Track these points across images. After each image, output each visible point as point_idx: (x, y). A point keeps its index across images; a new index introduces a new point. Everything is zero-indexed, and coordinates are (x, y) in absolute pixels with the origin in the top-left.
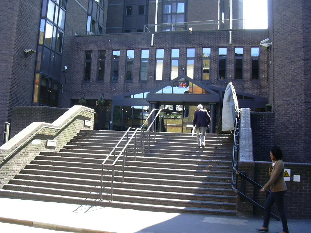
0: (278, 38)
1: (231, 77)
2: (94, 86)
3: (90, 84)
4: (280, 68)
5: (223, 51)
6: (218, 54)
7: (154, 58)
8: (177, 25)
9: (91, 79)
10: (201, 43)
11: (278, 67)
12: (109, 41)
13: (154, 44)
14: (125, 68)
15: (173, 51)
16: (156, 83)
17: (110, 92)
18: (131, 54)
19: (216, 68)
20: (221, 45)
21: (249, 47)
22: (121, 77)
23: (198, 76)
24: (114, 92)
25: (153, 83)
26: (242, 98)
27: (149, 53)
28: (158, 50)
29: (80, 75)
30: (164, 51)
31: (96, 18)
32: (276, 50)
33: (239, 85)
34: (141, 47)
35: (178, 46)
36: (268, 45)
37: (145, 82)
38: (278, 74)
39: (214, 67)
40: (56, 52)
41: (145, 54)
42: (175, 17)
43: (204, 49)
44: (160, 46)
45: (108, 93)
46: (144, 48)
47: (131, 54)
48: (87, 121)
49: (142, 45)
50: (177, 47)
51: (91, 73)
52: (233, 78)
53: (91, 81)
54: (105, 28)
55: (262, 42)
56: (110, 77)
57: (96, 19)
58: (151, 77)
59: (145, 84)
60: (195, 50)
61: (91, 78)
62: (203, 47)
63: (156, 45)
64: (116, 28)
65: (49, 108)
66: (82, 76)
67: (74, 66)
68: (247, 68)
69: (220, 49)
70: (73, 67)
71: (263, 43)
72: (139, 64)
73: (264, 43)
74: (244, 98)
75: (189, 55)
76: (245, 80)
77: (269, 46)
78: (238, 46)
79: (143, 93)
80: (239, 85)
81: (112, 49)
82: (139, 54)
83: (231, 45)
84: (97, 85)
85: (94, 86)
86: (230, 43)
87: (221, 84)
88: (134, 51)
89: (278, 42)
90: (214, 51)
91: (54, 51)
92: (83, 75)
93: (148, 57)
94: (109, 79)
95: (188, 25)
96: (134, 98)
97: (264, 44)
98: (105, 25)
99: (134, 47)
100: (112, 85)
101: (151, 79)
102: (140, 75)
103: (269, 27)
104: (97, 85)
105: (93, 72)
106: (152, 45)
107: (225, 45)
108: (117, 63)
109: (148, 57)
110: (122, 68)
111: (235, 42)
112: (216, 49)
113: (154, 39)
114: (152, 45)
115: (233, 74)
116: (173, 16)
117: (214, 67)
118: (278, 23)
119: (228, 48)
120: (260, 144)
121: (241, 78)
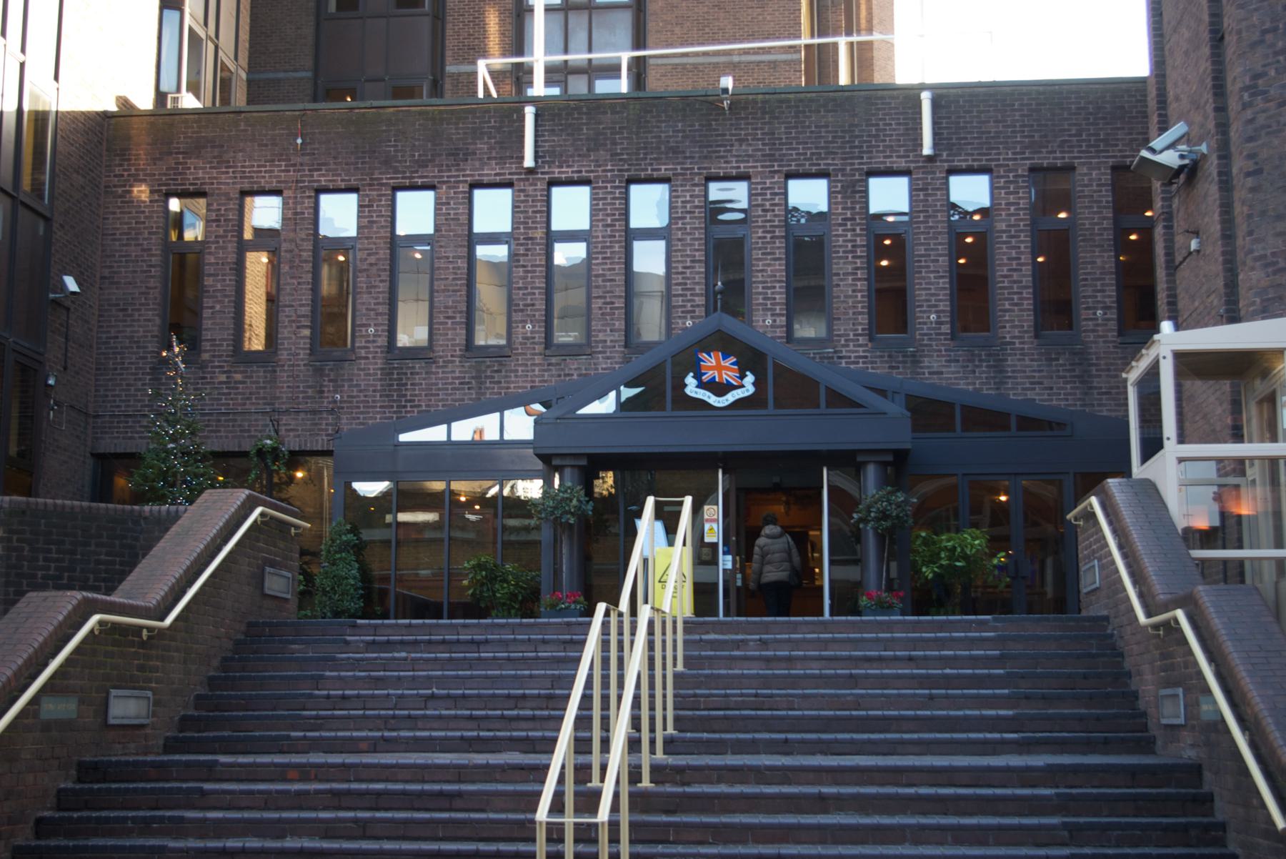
0: (1261, 119)
1: (937, 323)
2: (223, 378)
3: (201, 368)
4: (1275, 273)
5: (890, 196)
6: (867, 207)
7: (539, 234)
8: (594, 63)
9: (206, 345)
10: (777, 153)
11: (1267, 266)
12: (299, 141)
13: (536, 162)
14: (706, 285)
15: (638, 193)
16: (554, 360)
17: (314, 412)
18: (339, 215)
19: (859, 279)
20: (879, 161)
21: (1020, 172)
22: (372, 330)
23: (769, 321)
24: (332, 412)
25: (538, 360)
26: (1006, 427)
27: (515, 207)
28: (557, 192)
29: (149, 320)
30: (592, 194)
31: (202, 22)
32: (1250, 179)
33: (981, 361)
34: (470, 171)
35: (663, 170)
36: (1182, 157)
37: (498, 355)
38: (1268, 300)
39: (848, 274)
40: (22, 197)
41: (493, 210)
42: (586, 25)
43: (792, 184)
44: (567, 172)
45: (302, 416)
46: (486, 180)
47: (415, 213)
48: (272, 570)
49: (477, 164)
50: (655, 174)
51: (206, 313)
52: (946, 329)
53: (206, 356)
54: (244, 76)
55: (1157, 143)
56: (307, 332)
57: (206, 24)
58: (529, 326)
59: (501, 364)
60: (750, 189)
61: (207, 335)
62: (790, 176)
63: (550, 163)
64: (281, 75)
65: (123, 510)
66: (155, 328)
67: (106, 272)
68: (1015, 276)
69: (875, 184)
70: (103, 278)
71: (1161, 152)
72: (462, 264)
73: (1168, 148)
74: (1020, 428)
75: (638, 220)
76: (1008, 333)
77: (1186, 161)
78: (964, 165)
79: (498, 414)
80: (981, 361)
81: (315, 185)
82: (462, 209)
83: (930, 159)
84: (238, 377)
85: (223, 378)
86: (927, 150)
87: (890, 356)
88: (430, 195)
89: (1260, 142)
90: (844, 191)
91: (9, 189)
92: (158, 321)
93: (507, 227)
94: (305, 344)
95: (652, 61)
96: (506, 437)
97: (1166, 153)
98: (244, 60)
99: (431, 173)
100: (319, 372)
101: (527, 338)
102: (467, 318)
103: (1151, 71)
104: (238, 377)
105: (218, 307)
106: (529, 162)
107: (902, 164)
108: (899, 249)
109: (507, 227)
110: (375, 287)
111: (949, 147)
112: (854, 183)
113: (536, 136)
114: (529, 162)
115: (945, 306)
116: (573, 17)
117: (848, 274)
118: (1253, 45)
119: (286, 193)
120: (40, 574)
121: (1070, 327)
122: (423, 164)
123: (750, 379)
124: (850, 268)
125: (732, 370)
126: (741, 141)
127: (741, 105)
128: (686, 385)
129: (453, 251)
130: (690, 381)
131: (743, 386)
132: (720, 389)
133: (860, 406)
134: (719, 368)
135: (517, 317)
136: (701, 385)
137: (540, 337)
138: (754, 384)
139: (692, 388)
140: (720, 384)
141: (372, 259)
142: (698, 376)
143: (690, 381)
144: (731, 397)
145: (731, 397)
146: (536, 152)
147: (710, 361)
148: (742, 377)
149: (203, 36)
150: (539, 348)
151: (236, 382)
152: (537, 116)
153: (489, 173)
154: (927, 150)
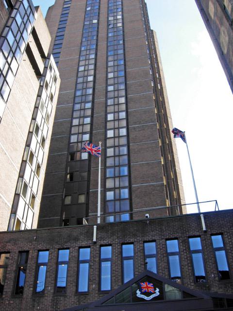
2: (8, 302)
9: (4, 293)
16: (101, 295)
20: (191, 233)
25: (96, 295)
34: (79, 244)
35: (132, 240)
44: (105, 242)
49: (81, 242)
50: (129, 241)
52: (217, 279)
53: (4, 296)
56: (32, 289)
57: (23, 219)
58: (94, 286)
78: (215, 232)
79: (33, 228)
84: (12, 302)
90: (182, 242)
99: (68, 245)
100: (34, 300)
104: (12, 302)
106: (95, 240)
111: (210, 228)
112: (185, 240)
113: (97, 235)
114: (95, 240)
122: (66, 242)
123: (158, 290)
124: (186, 263)
125: (152, 288)
126: (152, 231)
127: (152, 221)
128: (137, 294)
129: (73, 265)
130: (138, 292)
131: (155, 293)
132: (148, 294)
133: (195, 297)
134: (147, 287)
135: (91, 283)
136: (142, 293)
137: (97, 289)
138: (159, 292)
139: (139, 294)
140: (148, 292)
141: (51, 268)
142: (140, 290)
143: (138, 292)
144: (152, 297)
145: (152, 297)
146: (97, 238)
147: (144, 285)
148: (155, 290)
149: (22, 221)
150: (97, 292)
151: (11, 304)
152: (97, 229)
153: (84, 244)
154: (204, 229)
